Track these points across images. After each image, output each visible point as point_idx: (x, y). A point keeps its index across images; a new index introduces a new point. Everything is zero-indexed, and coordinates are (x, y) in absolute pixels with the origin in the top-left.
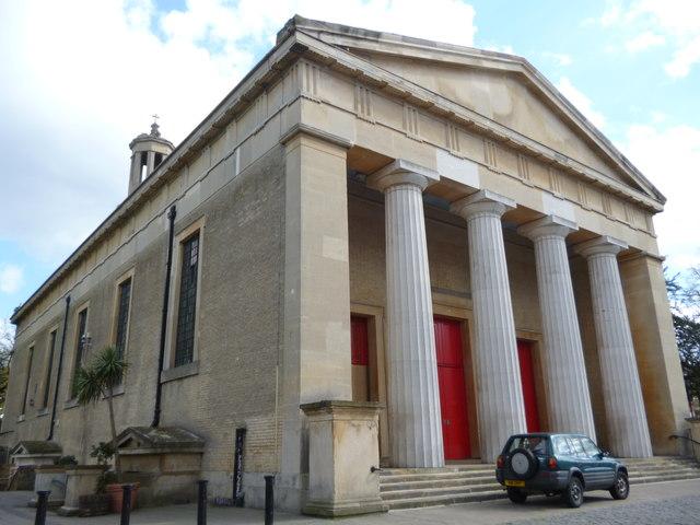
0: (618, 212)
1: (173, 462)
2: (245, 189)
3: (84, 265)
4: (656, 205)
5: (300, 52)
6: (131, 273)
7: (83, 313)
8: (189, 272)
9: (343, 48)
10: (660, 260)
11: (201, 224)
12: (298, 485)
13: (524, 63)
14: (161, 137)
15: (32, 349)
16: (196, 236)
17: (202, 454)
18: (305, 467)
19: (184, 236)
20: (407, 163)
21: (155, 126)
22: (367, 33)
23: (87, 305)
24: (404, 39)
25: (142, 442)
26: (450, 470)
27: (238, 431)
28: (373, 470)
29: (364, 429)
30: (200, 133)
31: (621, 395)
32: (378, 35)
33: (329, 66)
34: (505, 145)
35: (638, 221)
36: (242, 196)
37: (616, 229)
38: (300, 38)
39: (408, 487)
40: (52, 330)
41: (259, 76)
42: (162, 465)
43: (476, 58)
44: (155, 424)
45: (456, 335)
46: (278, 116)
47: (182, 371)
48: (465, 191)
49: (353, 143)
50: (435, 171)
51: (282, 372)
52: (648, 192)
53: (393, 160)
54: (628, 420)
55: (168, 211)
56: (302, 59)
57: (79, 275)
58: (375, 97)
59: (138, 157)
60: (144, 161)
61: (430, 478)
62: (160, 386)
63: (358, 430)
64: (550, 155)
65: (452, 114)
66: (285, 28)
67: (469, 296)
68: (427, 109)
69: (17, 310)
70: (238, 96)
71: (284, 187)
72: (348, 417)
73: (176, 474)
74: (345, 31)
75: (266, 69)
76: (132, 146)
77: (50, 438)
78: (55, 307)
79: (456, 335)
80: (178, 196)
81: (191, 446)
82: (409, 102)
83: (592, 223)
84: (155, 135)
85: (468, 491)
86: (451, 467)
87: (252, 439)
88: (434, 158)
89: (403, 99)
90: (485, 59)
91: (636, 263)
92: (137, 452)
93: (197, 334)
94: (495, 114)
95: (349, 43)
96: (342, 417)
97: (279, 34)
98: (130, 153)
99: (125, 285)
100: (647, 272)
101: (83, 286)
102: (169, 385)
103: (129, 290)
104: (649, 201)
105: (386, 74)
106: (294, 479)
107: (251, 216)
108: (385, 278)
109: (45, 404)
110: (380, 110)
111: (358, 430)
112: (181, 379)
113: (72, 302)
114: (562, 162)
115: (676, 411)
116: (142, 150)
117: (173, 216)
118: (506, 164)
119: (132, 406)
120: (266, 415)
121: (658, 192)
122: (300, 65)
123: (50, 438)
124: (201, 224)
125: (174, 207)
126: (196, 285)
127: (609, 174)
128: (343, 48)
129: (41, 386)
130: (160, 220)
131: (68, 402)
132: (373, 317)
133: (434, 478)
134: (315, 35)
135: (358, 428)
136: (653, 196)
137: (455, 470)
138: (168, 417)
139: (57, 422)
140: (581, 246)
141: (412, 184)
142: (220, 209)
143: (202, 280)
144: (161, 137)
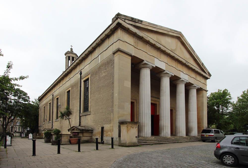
0: (199, 78)
1: (85, 134)
2: (102, 67)
3: (56, 86)
4: (208, 77)
5: (119, 26)
6: (70, 89)
7: (58, 99)
8: (86, 89)
9: (132, 25)
10: (207, 91)
11: (89, 76)
12: (118, 140)
13: (180, 33)
14: (74, 52)
15: (44, 107)
16: (88, 79)
17: (92, 132)
18: (120, 136)
19: (84, 79)
20: (147, 61)
21: (71, 49)
22: (139, 20)
23: (58, 97)
24: (149, 23)
25: (77, 129)
26: (152, 138)
27: (102, 127)
28: (136, 137)
29: (134, 128)
30: (88, 50)
31: (192, 122)
32: (142, 21)
33: (127, 30)
34: (173, 58)
35: (203, 80)
36: (101, 69)
37: (197, 81)
38: (119, 20)
39: (143, 141)
40: (50, 102)
41: (106, 33)
42: (83, 134)
43: (168, 31)
44: (80, 125)
45: (155, 107)
46: (112, 45)
47: (85, 113)
48: (162, 70)
49: (133, 55)
50: (154, 64)
51: (113, 114)
52: (207, 73)
53: (143, 60)
54: (193, 128)
55: (79, 72)
56: (119, 28)
57: (55, 89)
58: (139, 41)
59: (67, 58)
60: (69, 59)
61: (148, 139)
62: (80, 117)
63: (133, 128)
64: (184, 62)
65: (160, 48)
66: (115, 17)
67: (159, 99)
68: (153, 46)
69: (39, 97)
70: (100, 39)
71: (114, 66)
72: (131, 125)
73: (86, 136)
74: (133, 19)
75: (109, 30)
76: (65, 54)
77: (52, 128)
78: (49, 98)
79: (155, 107)
80: (82, 68)
81: (90, 131)
82: (149, 44)
83: (192, 81)
84: (71, 52)
85: (157, 142)
86: (153, 137)
87: (105, 129)
88: (154, 61)
89: (147, 42)
90: (170, 32)
91: (201, 91)
92: (76, 131)
93: (89, 105)
94: (171, 49)
95: (133, 23)
96: (129, 125)
97: (113, 19)
98: (65, 57)
99: (69, 92)
100: (203, 94)
101: (57, 92)
102: (82, 117)
103: (70, 93)
104: (207, 76)
105: (143, 34)
106: (117, 138)
107: (104, 74)
108: (139, 93)
109: (50, 120)
110: (141, 45)
111: (133, 128)
112: (86, 115)
113: (54, 96)
114: (187, 64)
115: (204, 126)
116: (70, 56)
117: (81, 74)
118: (173, 64)
119: (74, 121)
120: (109, 124)
121: (210, 74)
122: (119, 29)
123: (52, 128)
124: (89, 76)
125: (81, 71)
126: (88, 92)
127: (198, 68)
128: (132, 25)
129: (48, 116)
130: (77, 75)
131: (56, 120)
132: (134, 102)
133: (149, 139)
134: (124, 20)
135: (133, 128)
136: (208, 74)
137: (153, 137)
138: (82, 124)
139: (53, 124)
140: (188, 86)
141: (148, 68)
142: (95, 72)
143: (90, 91)
144: (74, 52)
